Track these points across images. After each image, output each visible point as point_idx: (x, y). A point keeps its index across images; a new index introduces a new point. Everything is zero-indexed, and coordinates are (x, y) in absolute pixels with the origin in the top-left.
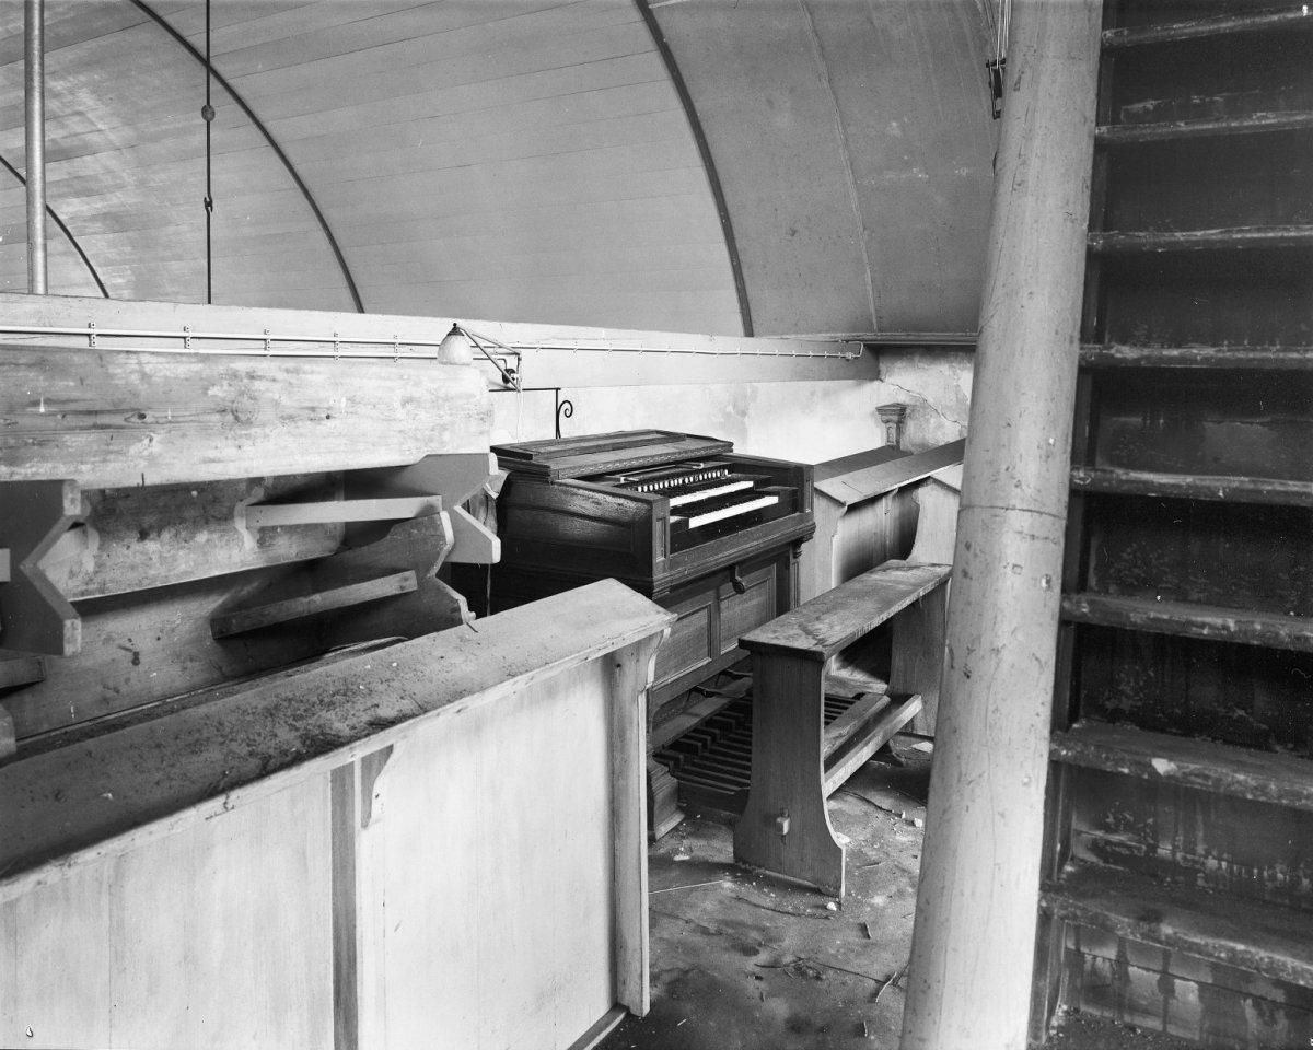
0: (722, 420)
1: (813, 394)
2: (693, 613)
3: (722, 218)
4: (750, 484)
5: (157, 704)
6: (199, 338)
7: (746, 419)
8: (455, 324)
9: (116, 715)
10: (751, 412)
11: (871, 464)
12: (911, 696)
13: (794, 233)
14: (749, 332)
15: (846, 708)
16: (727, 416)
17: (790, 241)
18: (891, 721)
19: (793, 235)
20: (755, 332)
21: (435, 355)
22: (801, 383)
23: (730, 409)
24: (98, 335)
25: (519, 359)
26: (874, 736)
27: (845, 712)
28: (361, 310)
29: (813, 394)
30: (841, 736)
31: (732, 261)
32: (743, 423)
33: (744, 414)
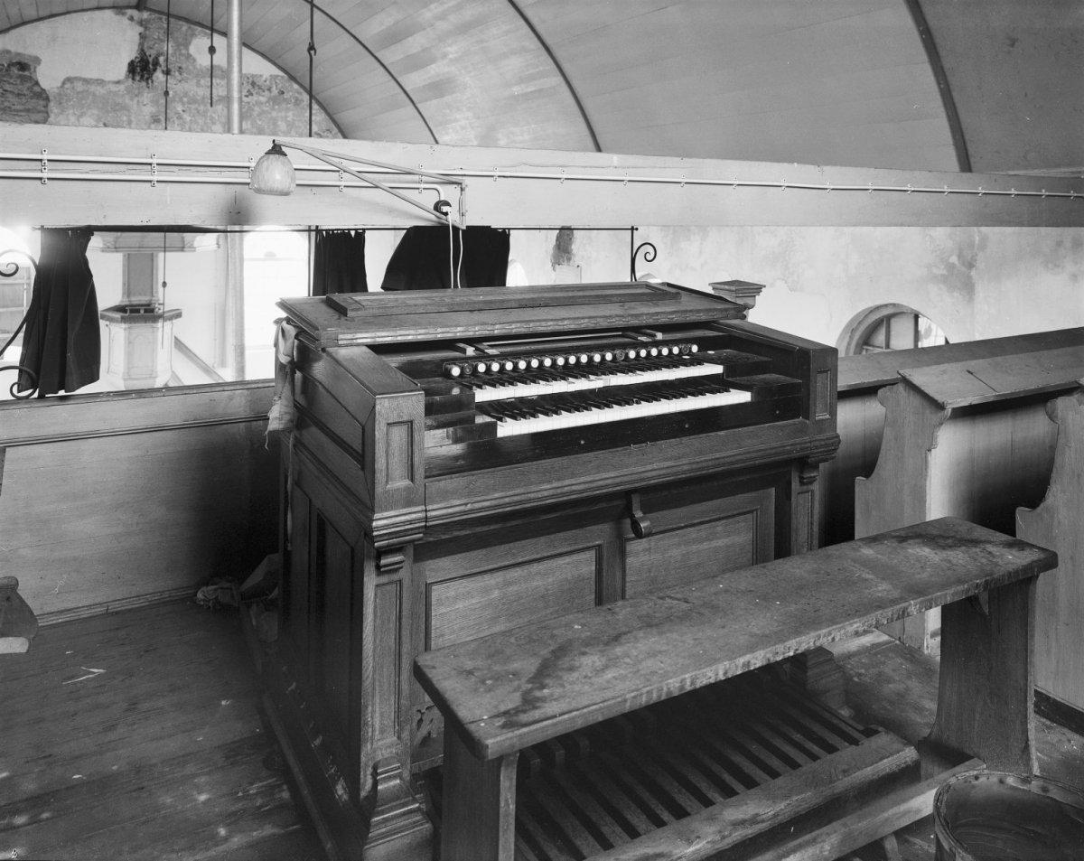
0: (945, 272)
1: (1059, 244)
2: (560, 555)
3: (921, 33)
4: (717, 369)
5: (289, 516)
6: (504, 177)
7: (973, 273)
8: (274, 141)
9: (508, 494)
10: (980, 264)
11: (1049, 347)
12: (969, 758)
13: (1013, 42)
14: (966, 165)
15: (814, 758)
16: (951, 267)
17: (1009, 52)
18: (904, 801)
19: (1013, 45)
20: (973, 169)
21: (249, 181)
22: (1043, 230)
23: (954, 259)
24: (629, 181)
25: (462, 190)
26: (814, 841)
27: (808, 767)
28: (599, 149)
29: (1059, 244)
30: (754, 820)
31: (939, 84)
32: (970, 277)
33: (971, 266)
